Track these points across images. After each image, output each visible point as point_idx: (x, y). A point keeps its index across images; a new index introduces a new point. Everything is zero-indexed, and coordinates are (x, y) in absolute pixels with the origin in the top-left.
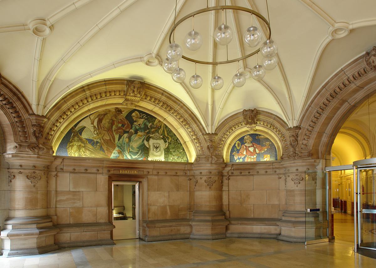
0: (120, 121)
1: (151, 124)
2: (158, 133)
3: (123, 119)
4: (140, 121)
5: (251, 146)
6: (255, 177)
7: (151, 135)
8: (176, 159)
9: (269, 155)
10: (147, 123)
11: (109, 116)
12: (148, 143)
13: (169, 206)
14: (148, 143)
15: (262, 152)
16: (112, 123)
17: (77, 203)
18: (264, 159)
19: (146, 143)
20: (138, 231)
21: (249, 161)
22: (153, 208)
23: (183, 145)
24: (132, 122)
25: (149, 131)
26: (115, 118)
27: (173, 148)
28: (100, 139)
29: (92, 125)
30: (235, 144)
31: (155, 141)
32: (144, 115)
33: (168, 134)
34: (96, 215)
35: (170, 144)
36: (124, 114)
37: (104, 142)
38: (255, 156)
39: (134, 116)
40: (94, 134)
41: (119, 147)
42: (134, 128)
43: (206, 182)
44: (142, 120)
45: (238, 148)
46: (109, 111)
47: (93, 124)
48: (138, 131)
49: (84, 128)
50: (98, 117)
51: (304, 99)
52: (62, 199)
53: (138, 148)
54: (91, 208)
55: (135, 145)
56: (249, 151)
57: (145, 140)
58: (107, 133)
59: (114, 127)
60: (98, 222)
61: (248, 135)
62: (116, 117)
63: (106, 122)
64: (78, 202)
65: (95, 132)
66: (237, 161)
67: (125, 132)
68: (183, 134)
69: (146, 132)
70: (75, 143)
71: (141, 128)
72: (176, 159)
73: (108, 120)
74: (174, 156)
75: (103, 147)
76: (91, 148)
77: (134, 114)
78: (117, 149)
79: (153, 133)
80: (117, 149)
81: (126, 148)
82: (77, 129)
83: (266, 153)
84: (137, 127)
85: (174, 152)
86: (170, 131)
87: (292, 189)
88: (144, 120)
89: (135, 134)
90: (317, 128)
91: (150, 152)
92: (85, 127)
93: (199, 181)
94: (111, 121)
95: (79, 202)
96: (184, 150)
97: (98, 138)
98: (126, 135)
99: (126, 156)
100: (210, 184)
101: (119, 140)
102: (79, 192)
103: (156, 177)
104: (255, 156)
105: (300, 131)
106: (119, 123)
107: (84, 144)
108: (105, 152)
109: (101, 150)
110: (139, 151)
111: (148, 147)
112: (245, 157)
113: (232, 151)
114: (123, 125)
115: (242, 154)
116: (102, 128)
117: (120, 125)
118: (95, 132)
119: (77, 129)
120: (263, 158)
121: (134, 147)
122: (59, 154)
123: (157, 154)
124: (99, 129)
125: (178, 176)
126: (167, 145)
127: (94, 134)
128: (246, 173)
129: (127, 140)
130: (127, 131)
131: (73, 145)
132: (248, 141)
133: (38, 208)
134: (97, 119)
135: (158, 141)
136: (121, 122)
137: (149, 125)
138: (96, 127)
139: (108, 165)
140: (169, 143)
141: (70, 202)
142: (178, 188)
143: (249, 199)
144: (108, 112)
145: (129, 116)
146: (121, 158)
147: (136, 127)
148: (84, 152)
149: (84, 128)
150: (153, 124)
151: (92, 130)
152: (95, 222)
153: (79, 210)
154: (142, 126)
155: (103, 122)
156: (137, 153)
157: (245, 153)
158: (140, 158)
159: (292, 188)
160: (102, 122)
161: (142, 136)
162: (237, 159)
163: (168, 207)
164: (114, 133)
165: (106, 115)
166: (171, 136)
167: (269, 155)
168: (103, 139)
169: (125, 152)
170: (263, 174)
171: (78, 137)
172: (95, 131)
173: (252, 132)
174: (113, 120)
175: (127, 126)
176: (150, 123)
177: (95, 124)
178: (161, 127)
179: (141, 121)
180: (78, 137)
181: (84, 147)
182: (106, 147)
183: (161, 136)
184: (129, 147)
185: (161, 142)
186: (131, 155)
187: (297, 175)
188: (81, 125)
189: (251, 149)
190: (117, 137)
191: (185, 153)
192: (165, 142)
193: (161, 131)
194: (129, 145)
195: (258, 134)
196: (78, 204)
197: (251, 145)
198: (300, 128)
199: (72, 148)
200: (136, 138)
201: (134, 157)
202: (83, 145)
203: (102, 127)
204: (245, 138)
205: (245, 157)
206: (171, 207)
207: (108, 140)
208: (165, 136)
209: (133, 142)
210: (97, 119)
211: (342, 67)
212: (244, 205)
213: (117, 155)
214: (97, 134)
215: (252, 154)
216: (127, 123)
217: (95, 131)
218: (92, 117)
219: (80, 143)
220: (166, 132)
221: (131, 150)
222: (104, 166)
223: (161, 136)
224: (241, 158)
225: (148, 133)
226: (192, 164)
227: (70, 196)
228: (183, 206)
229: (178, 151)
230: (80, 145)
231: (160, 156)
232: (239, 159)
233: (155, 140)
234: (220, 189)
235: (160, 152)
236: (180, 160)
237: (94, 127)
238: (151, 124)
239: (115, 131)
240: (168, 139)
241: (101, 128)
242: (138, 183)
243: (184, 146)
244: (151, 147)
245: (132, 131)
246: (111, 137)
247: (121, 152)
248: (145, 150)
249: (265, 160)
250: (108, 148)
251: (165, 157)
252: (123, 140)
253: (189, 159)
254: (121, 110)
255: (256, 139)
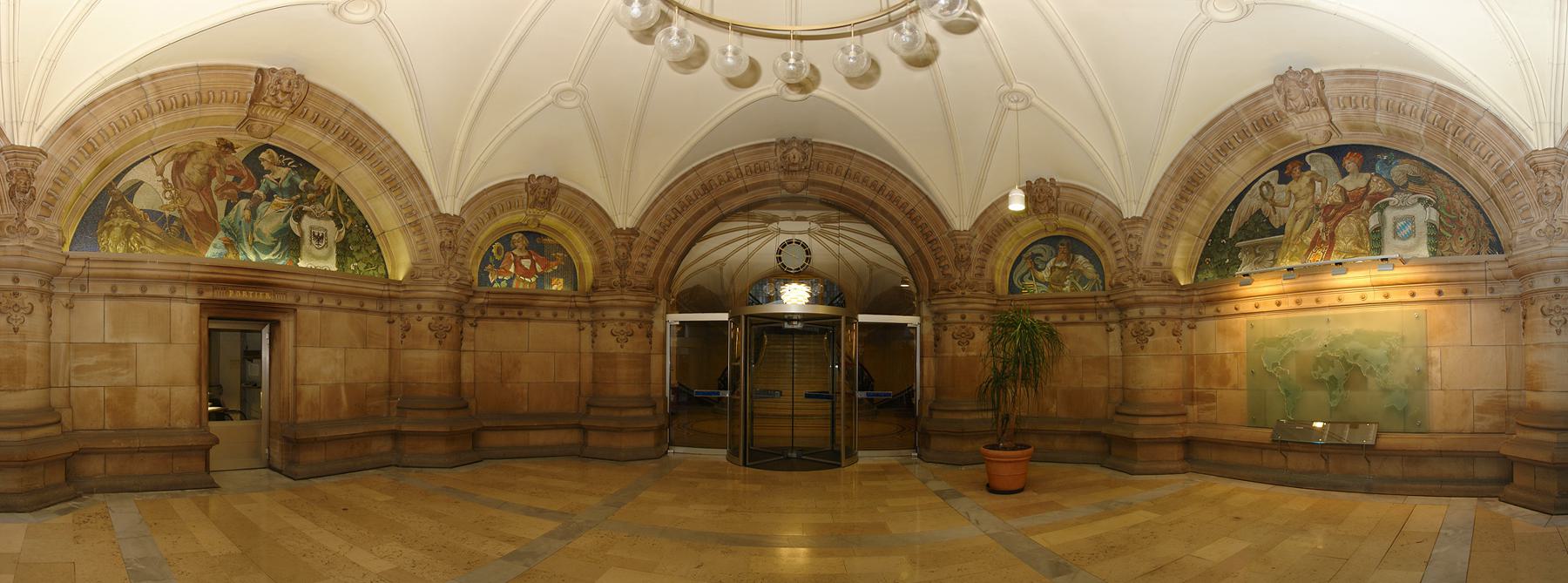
0: (230, 169)
1: (305, 181)
2: (323, 204)
3: (237, 164)
4: (279, 173)
5: (527, 258)
6: (532, 324)
7: (306, 208)
8: (362, 268)
9: (561, 280)
10: (298, 179)
11: (202, 157)
12: (299, 225)
13: (346, 384)
14: (299, 225)
15: (549, 271)
16: (211, 173)
17: (123, 375)
18: (552, 286)
19: (293, 224)
20: (267, 450)
21: (521, 286)
22: (308, 391)
23: (377, 238)
24: (260, 173)
25: (301, 198)
26: (219, 162)
27: (356, 243)
28: (180, 211)
29: (160, 178)
30: (491, 248)
31: (315, 222)
32: (290, 161)
33: (345, 210)
34: (167, 408)
35: (348, 231)
36: (241, 153)
37: (191, 219)
38: (533, 279)
39: (264, 160)
40: (166, 198)
41: (226, 230)
42: (263, 186)
43: (430, 329)
44: (285, 170)
45: (498, 258)
46: (203, 147)
47: (162, 175)
48: (275, 196)
49: (137, 185)
50: (173, 157)
51: (658, 180)
52: (86, 363)
53: (274, 235)
54: (156, 388)
55: (268, 227)
56: (521, 265)
57: (291, 219)
58: (197, 196)
59: (215, 183)
60: (172, 426)
61: (519, 232)
62: (218, 158)
63: (193, 171)
64: (125, 372)
65: (168, 194)
66: (496, 285)
67: (242, 195)
68: (383, 212)
69: (294, 198)
70: (116, 220)
71: (280, 189)
72: (362, 268)
73: (199, 166)
74: (357, 262)
75: (187, 230)
76: (154, 230)
77: (263, 155)
78: (221, 234)
79: (311, 202)
80: (221, 234)
81: (244, 234)
82: (122, 185)
83: (556, 274)
84: (273, 186)
85: (358, 251)
86: (349, 204)
87: (611, 351)
88: (289, 172)
89: (266, 200)
90: (666, 240)
91: (304, 247)
92: (141, 183)
93: (414, 324)
94: (207, 168)
95: (128, 373)
96: (379, 251)
97: (175, 209)
98: (244, 203)
99: (245, 253)
100: (439, 334)
101: (226, 214)
102: (126, 345)
103: (317, 312)
104: (533, 279)
105: (637, 239)
106: (227, 172)
107: (140, 222)
108: (191, 243)
109: (181, 237)
110: (277, 243)
111: (298, 234)
112: (512, 279)
113: (485, 262)
114: (237, 179)
115: (507, 272)
116: (184, 184)
117: (230, 178)
118: (168, 194)
119: (122, 185)
120: (550, 284)
121: (264, 231)
122: (73, 254)
123: (320, 253)
124: (176, 187)
125: (366, 311)
126: (343, 234)
127: (166, 198)
128: (514, 313)
129: (247, 213)
130: (248, 194)
131: (111, 226)
132: (520, 245)
133: (27, 387)
134: (172, 163)
135: (322, 223)
136: (233, 170)
137: (302, 183)
138: (170, 181)
139: (199, 275)
140: (346, 229)
141: (107, 371)
142: (366, 340)
143: (520, 370)
144: (199, 149)
145: (252, 159)
146: (231, 256)
147: (268, 186)
148: (140, 244)
149: (137, 185)
150: (311, 182)
151: (160, 189)
152: (166, 426)
153: (126, 395)
154: (285, 184)
155: (188, 169)
156: (272, 248)
157: (512, 270)
158: (279, 260)
159: (611, 349)
160: (186, 172)
161: (283, 207)
162: (494, 282)
163: (343, 388)
164: (215, 197)
165: (195, 156)
166: (353, 216)
167: (561, 280)
168: (186, 210)
169: (243, 243)
170: (550, 320)
171: (125, 206)
172: (165, 191)
173: (532, 228)
174: (213, 165)
175: (247, 182)
176: (302, 179)
177: (168, 174)
178: (329, 191)
179: (282, 172)
180: (125, 206)
181: (140, 230)
182: (195, 231)
183: (330, 213)
184: (252, 233)
185: (330, 225)
186: (256, 253)
187: (622, 324)
188: (131, 176)
189: (526, 263)
190: (221, 206)
191: (382, 257)
192: (339, 226)
193: (329, 199)
194: (252, 228)
195: (540, 234)
196: (125, 378)
197: (525, 254)
198: (638, 235)
199: (108, 235)
200: (270, 211)
201: (264, 258)
202: (136, 225)
203: (183, 180)
204: (514, 237)
205: (512, 279)
206: (349, 386)
207: (201, 212)
208: (339, 212)
209: (261, 219)
210: (172, 163)
211: (734, 148)
212: (509, 386)
213: (223, 251)
214: (173, 198)
215: (528, 274)
216: (248, 173)
217: (165, 191)
218: (159, 159)
219: (128, 222)
220: (340, 205)
221: (257, 239)
222: (191, 278)
223: (330, 213)
224: (503, 280)
225: (298, 202)
226: (398, 284)
227: (105, 357)
228: (375, 385)
229: (367, 251)
230: (129, 226)
231: (326, 258)
232: (499, 281)
233: (315, 220)
234: (458, 348)
235: (325, 250)
236: (371, 273)
237: (165, 182)
238: (305, 181)
239: (216, 191)
240: (346, 220)
241: (182, 184)
242: (267, 327)
243: (380, 241)
244: (307, 236)
245: (260, 193)
246: (207, 206)
247: (233, 243)
248: (290, 242)
249: (554, 288)
250: (200, 233)
251: (338, 264)
252: (236, 215)
253: (389, 271)
254: (232, 144)
255: (536, 241)
